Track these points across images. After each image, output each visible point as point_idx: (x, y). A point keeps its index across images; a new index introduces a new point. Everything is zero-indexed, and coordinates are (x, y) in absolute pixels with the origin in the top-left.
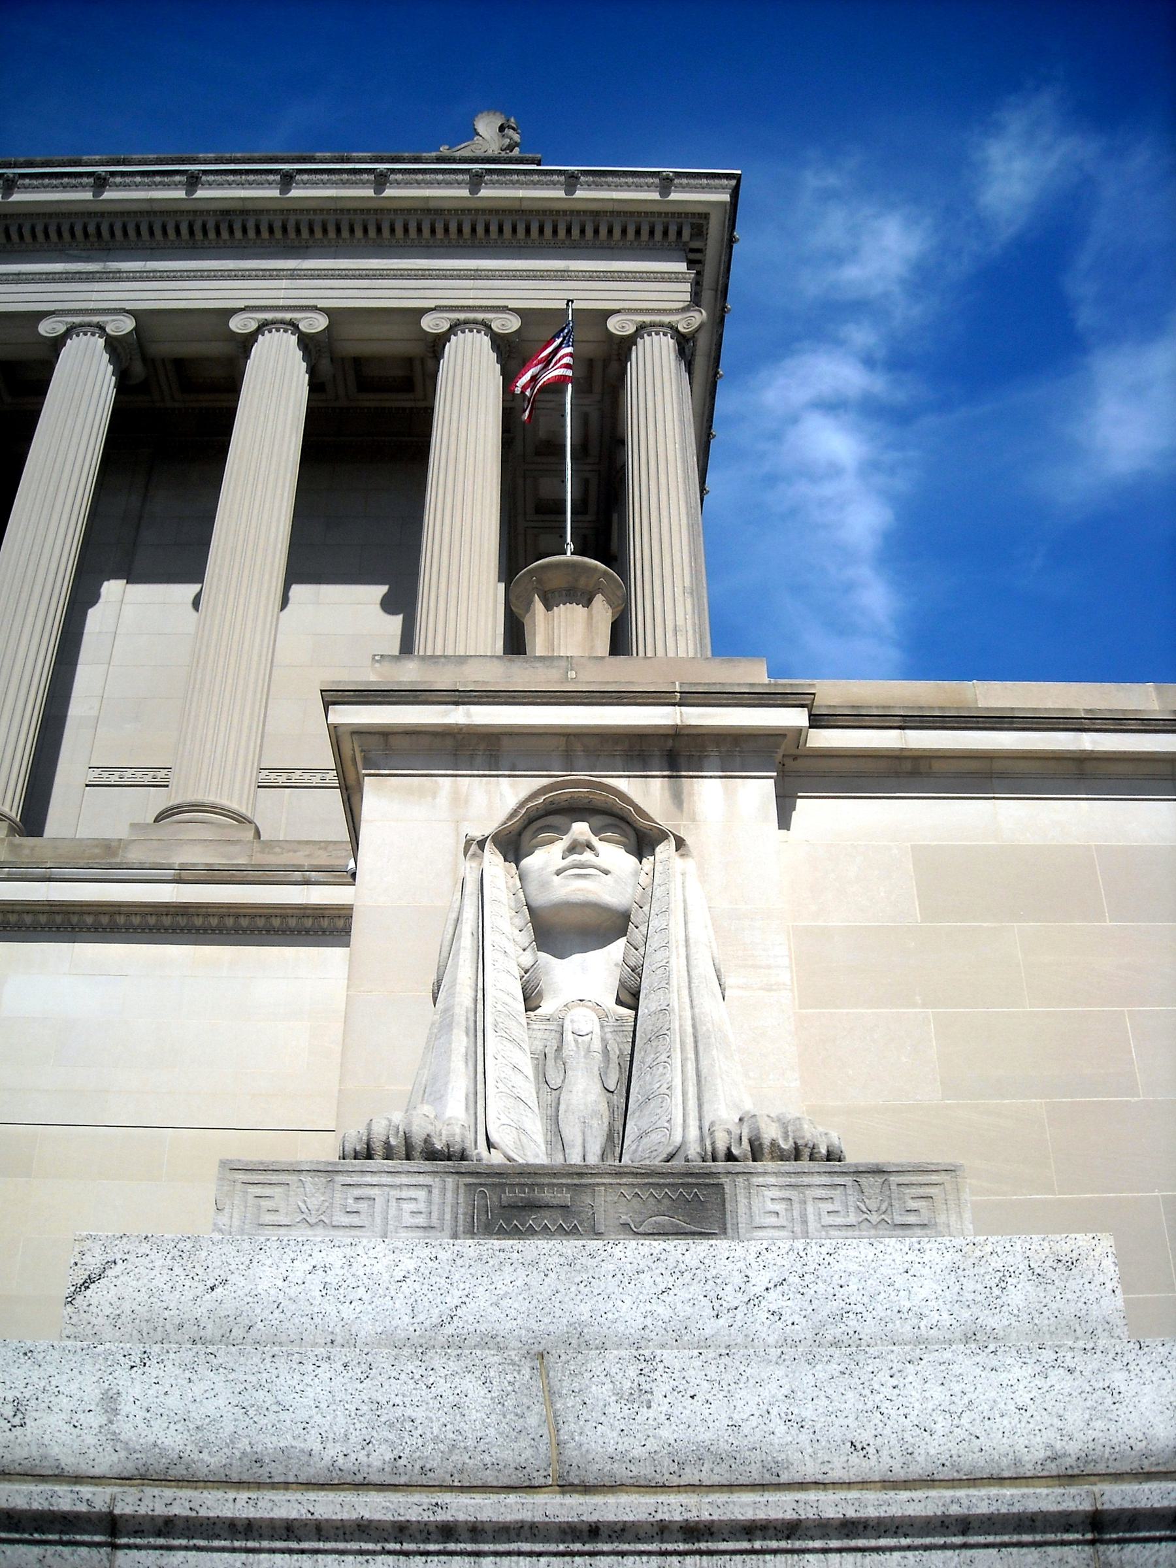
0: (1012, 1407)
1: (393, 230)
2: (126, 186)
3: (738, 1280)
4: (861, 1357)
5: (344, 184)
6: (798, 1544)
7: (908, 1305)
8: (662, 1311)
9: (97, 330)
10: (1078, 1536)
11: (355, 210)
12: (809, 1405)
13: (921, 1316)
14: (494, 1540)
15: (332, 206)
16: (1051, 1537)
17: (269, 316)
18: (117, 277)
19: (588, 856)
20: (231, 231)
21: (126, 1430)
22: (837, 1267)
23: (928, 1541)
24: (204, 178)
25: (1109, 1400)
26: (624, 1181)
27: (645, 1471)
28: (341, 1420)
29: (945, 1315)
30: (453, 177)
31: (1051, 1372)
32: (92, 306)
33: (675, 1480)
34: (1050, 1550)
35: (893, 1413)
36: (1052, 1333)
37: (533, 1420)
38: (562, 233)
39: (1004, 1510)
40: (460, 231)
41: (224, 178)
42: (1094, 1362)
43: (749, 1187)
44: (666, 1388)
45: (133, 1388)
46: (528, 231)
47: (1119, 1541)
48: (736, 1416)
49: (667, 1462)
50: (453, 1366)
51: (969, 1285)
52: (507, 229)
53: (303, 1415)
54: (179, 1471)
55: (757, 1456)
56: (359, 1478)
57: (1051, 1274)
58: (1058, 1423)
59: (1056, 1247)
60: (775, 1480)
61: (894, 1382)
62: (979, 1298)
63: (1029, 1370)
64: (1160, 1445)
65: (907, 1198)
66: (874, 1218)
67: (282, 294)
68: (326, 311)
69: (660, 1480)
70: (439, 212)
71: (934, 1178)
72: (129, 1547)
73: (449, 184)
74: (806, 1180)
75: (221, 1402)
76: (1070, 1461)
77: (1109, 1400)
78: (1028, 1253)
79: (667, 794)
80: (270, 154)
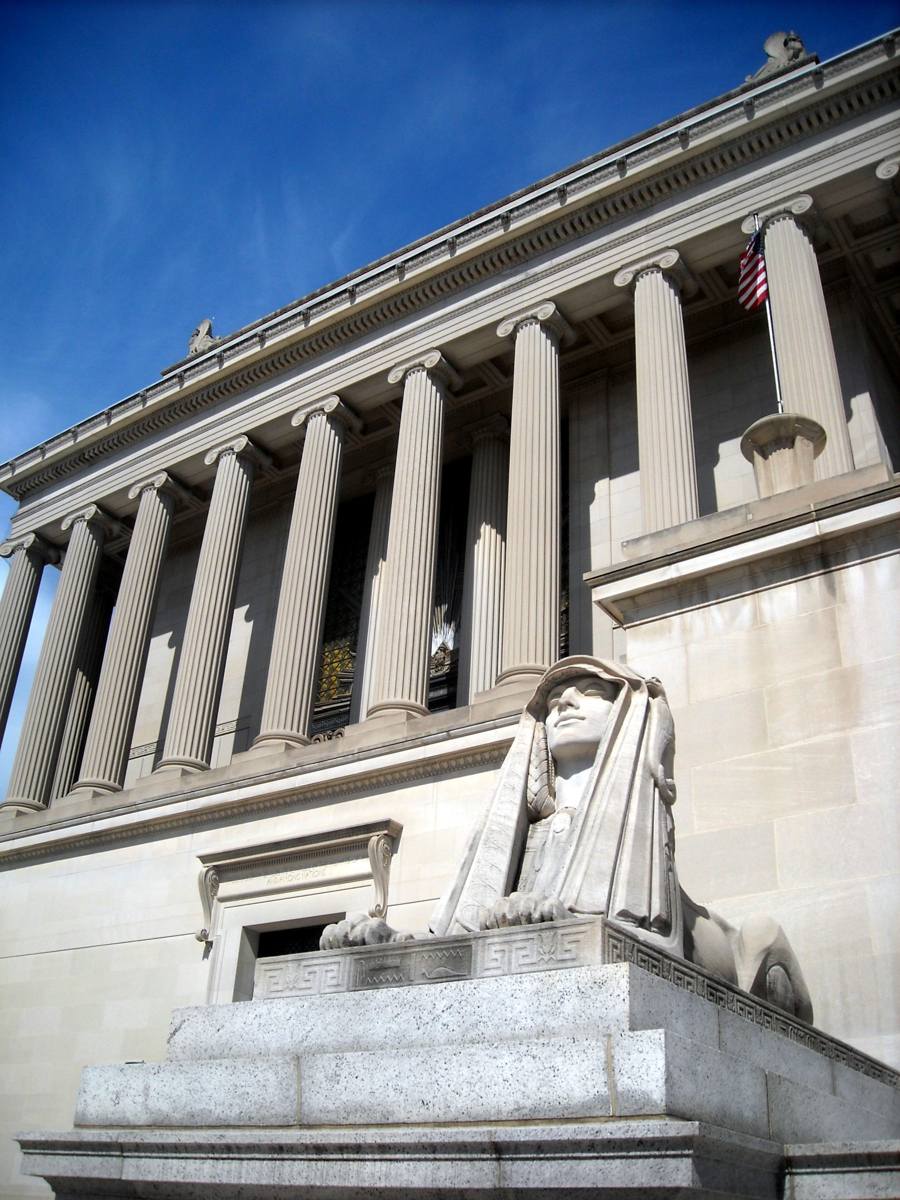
0: (501, 1080)
1: (705, 169)
2: (522, 216)
3: (430, 1007)
4: (432, 1053)
5: (660, 152)
6: (362, 1156)
7: (510, 1015)
8: (394, 1027)
9: (533, 320)
10: (489, 1156)
11: (675, 166)
12: (406, 1081)
13: (516, 1022)
14: (246, 1153)
15: (658, 170)
16: (475, 1156)
17: (638, 267)
18: (535, 279)
19: (570, 711)
20: (599, 217)
21: (150, 1103)
22: (477, 995)
23: (417, 1156)
24: (568, 189)
25: (552, 1074)
26: (425, 949)
27: (333, 1117)
28: (223, 1095)
29: (529, 1020)
30: (732, 113)
31: (524, 1059)
32: (525, 305)
33: (345, 1122)
34: (477, 1163)
35: (443, 1084)
36: (585, 1029)
37: (292, 1092)
38: (825, 118)
39: (446, 1141)
40: (751, 149)
41: (581, 183)
42: (547, 1051)
43: (483, 946)
44: (346, 1073)
45: (155, 1083)
46: (800, 127)
47: (512, 1159)
48: (374, 1088)
49: (343, 1112)
50: (265, 1066)
51: (544, 1001)
52: (784, 133)
53: (209, 1093)
54: (166, 1122)
55: (380, 1108)
56: (226, 1123)
57: (590, 992)
58: (523, 1089)
59: (594, 974)
60: (386, 1121)
61: (446, 1066)
62: (548, 1009)
63: (513, 1058)
64: (575, 1101)
65: (566, 943)
66: (546, 957)
67: (644, 246)
68: (676, 247)
69: (339, 1122)
70: (732, 142)
71: (582, 928)
72: (128, 1157)
73: (731, 119)
74: (514, 937)
75: (182, 1088)
76: (526, 1111)
77: (552, 1074)
78: (579, 979)
79: (824, 587)
80: (628, 139)
